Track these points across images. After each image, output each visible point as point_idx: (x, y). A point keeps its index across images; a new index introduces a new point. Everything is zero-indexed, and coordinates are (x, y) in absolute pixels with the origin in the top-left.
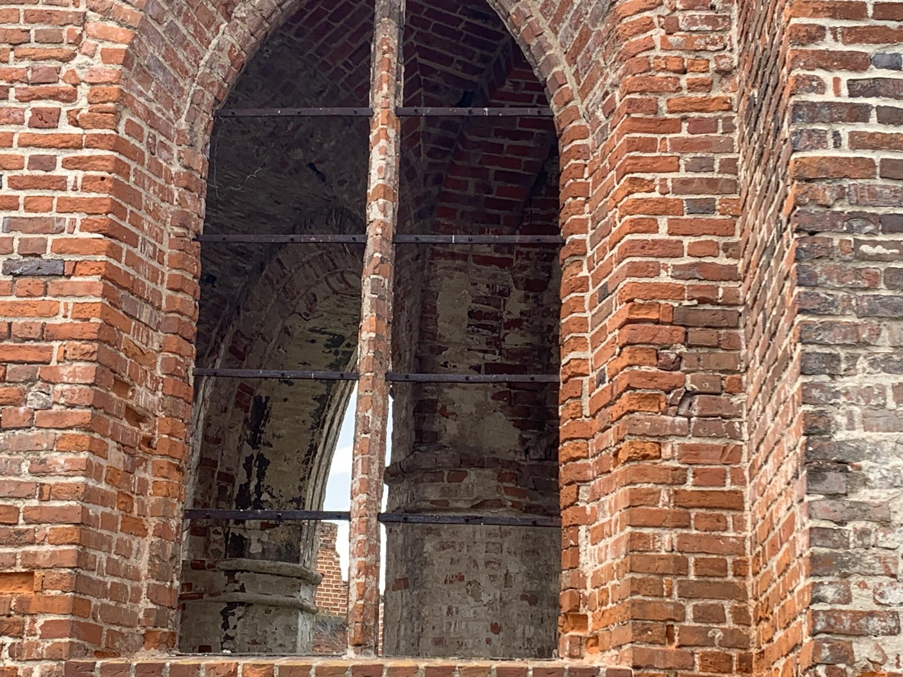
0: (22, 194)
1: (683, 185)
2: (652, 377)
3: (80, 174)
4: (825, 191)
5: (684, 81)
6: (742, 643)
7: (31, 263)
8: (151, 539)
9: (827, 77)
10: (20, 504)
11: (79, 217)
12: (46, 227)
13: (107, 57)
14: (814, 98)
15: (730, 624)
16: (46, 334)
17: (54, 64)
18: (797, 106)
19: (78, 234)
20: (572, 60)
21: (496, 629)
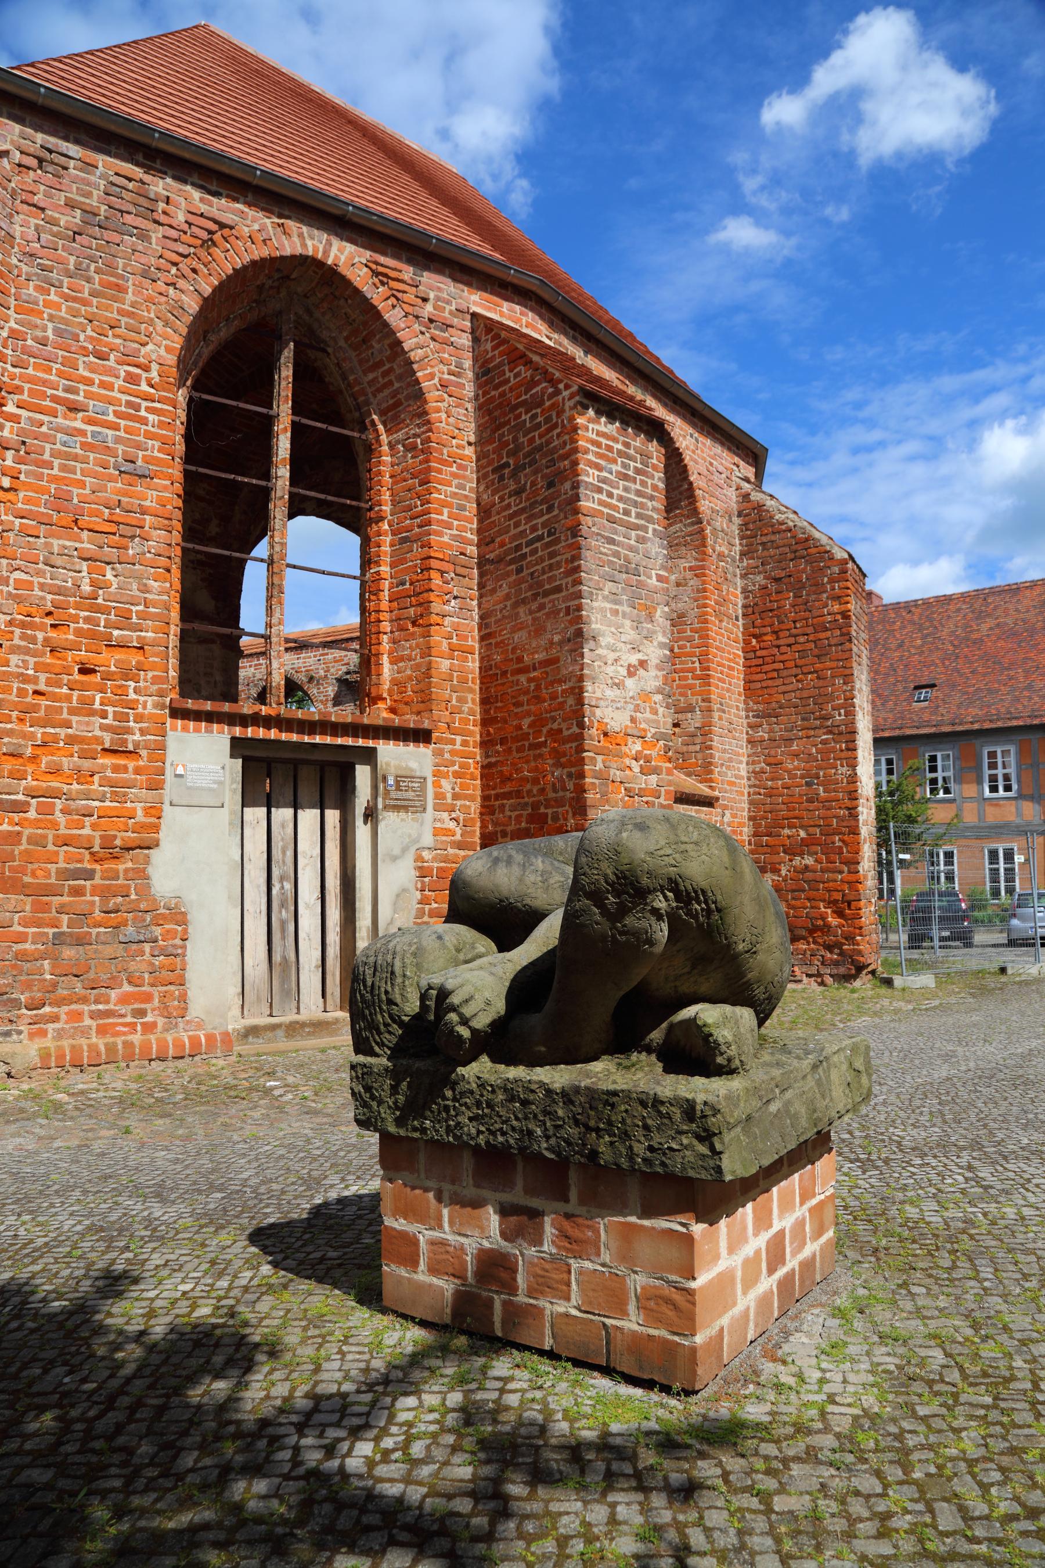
0: (123, 423)
1: (454, 495)
7: (127, 467)
11: (157, 444)
12: (139, 446)
13: (168, 349)
19: (156, 454)
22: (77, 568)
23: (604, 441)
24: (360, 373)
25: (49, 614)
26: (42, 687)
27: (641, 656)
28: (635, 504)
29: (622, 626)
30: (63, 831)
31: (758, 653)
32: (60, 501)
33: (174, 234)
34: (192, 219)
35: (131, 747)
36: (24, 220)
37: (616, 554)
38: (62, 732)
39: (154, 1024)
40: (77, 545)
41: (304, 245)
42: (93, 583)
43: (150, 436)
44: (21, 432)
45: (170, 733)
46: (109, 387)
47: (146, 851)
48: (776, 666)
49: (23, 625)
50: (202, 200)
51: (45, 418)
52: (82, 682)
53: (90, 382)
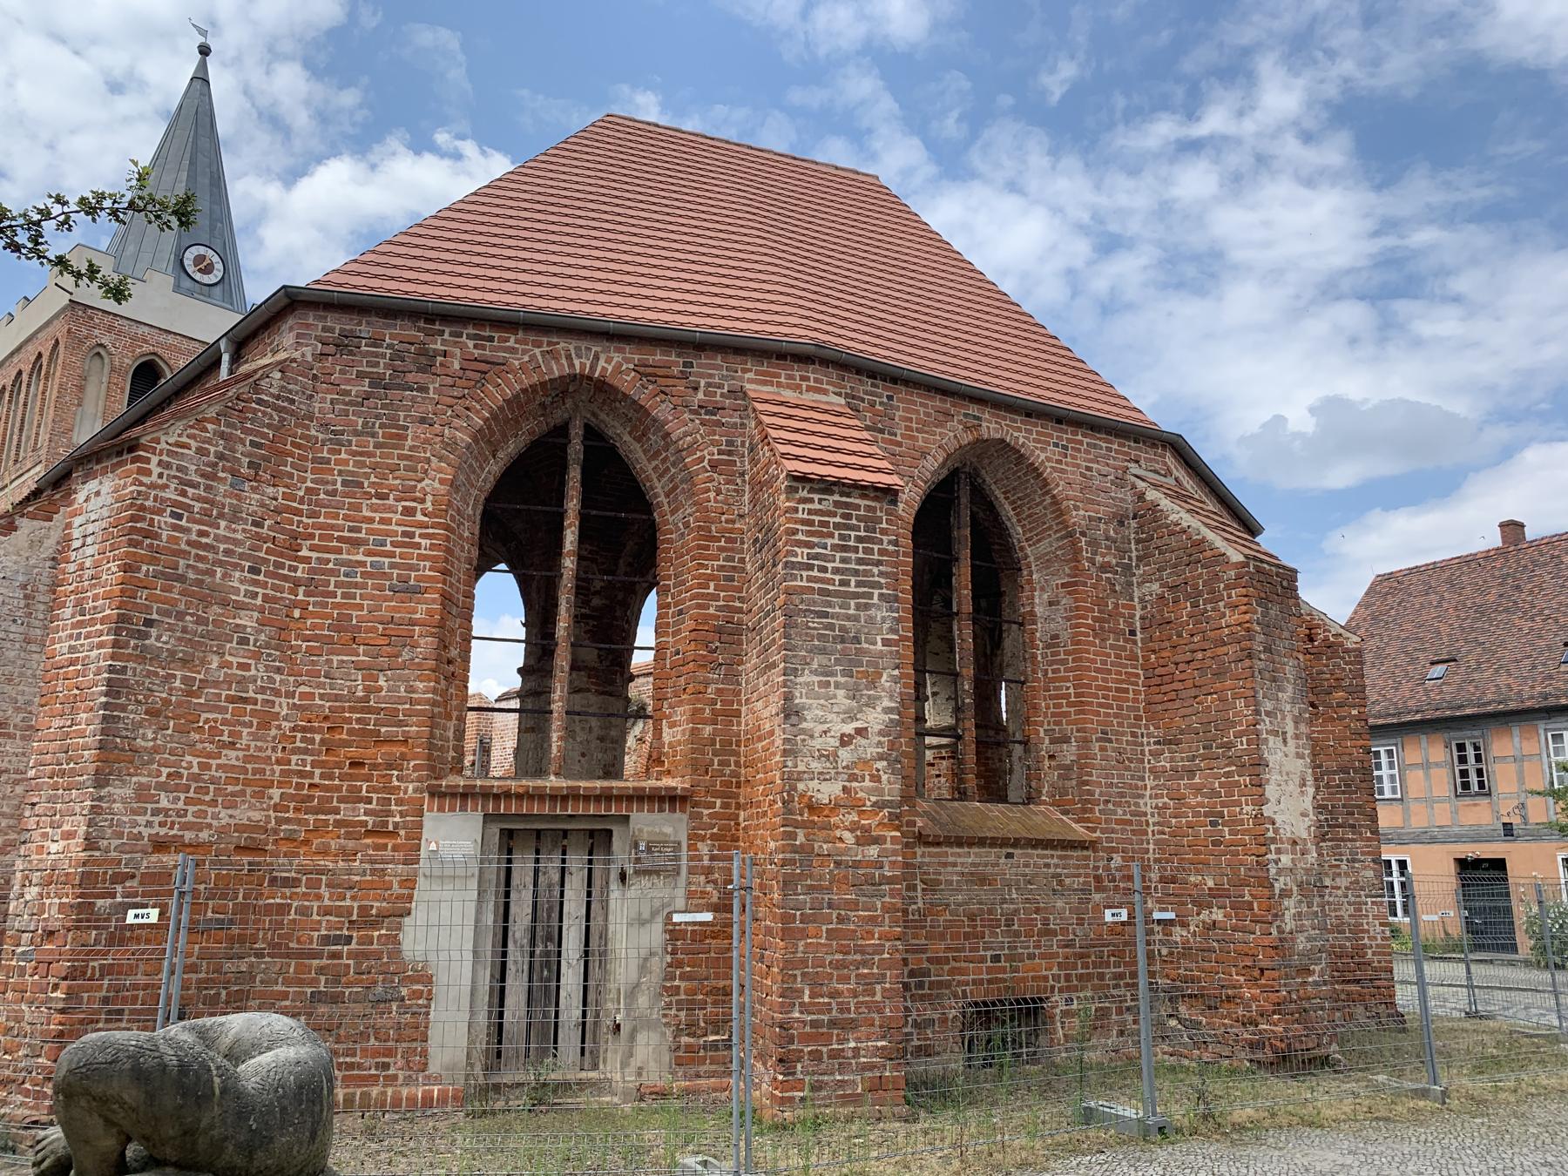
0: (398, 550)
1: (721, 568)
2: (704, 656)
3: (428, 542)
4: (796, 599)
5: (723, 518)
6: (736, 774)
8: (454, 722)
9: (799, 550)
10: (400, 707)
11: (428, 564)
12: (412, 568)
13: (442, 481)
14: (793, 559)
15: (733, 767)
16: (413, 623)
17: (413, 483)
18: (787, 562)
19: (427, 573)
20: (667, 496)
21: (583, 755)
22: (353, 677)
23: (817, 518)
24: (646, 462)
25: (326, 718)
26: (317, 780)
27: (858, 724)
28: (856, 573)
29: (835, 696)
30: (327, 902)
31: (1157, 672)
32: (341, 624)
33: (449, 381)
34: (466, 365)
35: (391, 828)
36: (322, 398)
37: (831, 627)
38: (331, 818)
39: (395, 1077)
40: (354, 659)
41: (572, 365)
42: (366, 689)
43: (421, 557)
44: (312, 571)
45: (426, 813)
46: (388, 521)
47: (398, 919)
48: (1176, 686)
49: (304, 730)
50: (475, 346)
51: (332, 557)
52: (350, 774)
53: (371, 520)
